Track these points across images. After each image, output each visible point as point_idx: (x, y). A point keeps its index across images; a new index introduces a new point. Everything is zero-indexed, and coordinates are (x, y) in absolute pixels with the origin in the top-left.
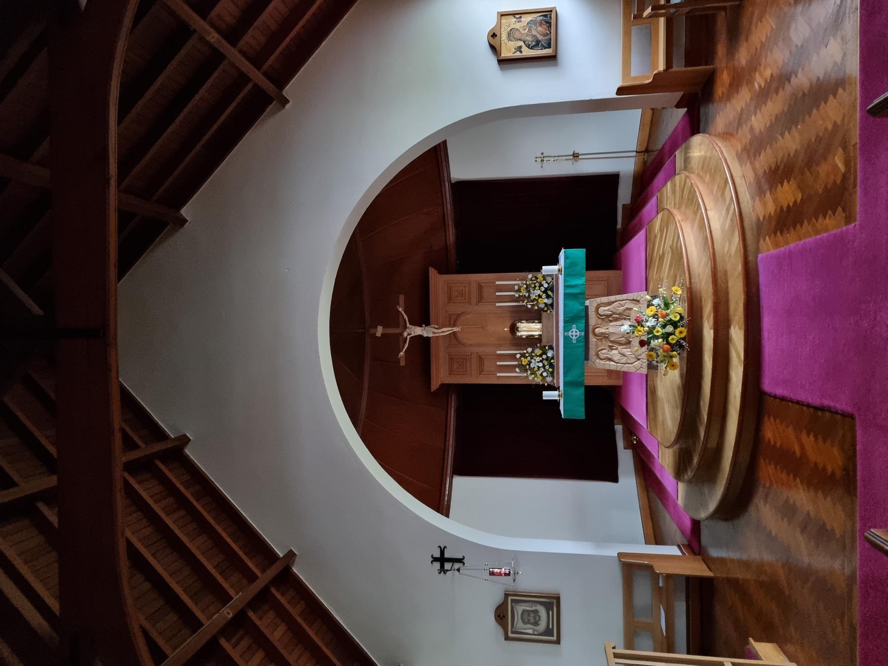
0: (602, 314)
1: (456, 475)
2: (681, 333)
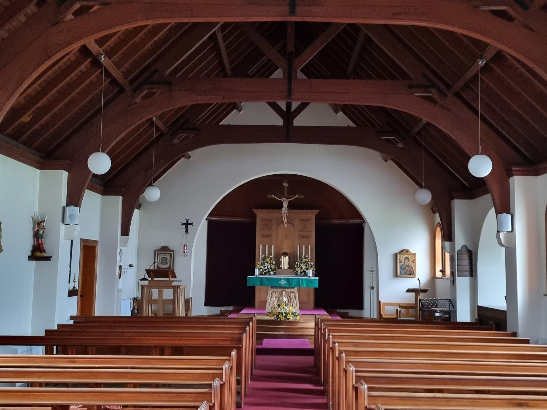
0: (291, 294)
1: (209, 222)
2: (283, 318)
